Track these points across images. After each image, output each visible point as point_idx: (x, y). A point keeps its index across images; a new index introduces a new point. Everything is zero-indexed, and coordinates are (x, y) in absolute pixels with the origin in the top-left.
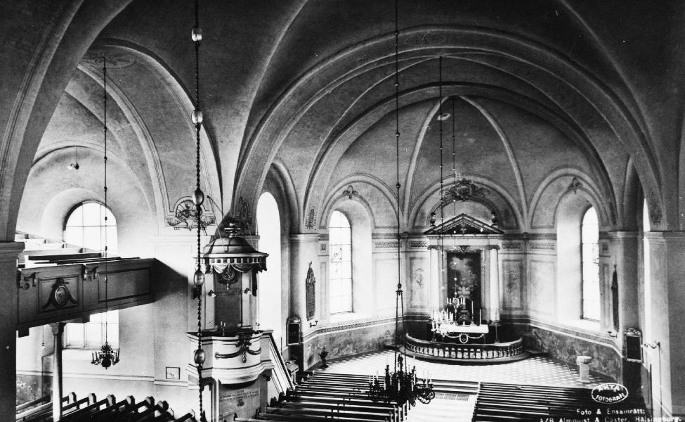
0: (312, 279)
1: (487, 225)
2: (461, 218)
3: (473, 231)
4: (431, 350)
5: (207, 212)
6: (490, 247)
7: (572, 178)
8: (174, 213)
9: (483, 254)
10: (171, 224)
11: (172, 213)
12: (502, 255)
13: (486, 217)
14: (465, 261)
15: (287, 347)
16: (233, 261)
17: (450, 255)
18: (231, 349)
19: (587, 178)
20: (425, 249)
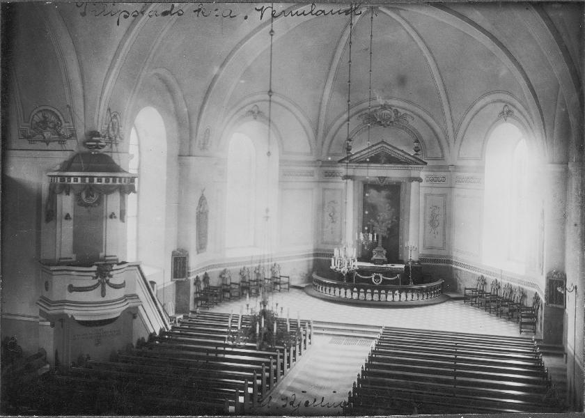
0: (204, 208)
1: (409, 155)
3: (392, 160)
4: (337, 290)
5: (67, 124)
6: (411, 179)
7: (504, 104)
9: (403, 187)
13: (408, 145)
14: (384, 193)
16: (85, 180)
17: (367, 186)
19: (519, 106)
20: (340, 179)
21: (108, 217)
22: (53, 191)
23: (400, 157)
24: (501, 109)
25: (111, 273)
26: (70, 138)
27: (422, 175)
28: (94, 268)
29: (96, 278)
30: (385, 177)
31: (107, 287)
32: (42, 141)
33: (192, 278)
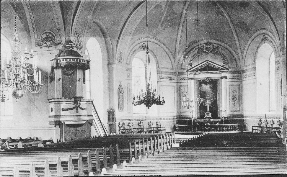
2: (206, 62)
5: (57, 38)
6: (222, 78)
8: (40, 39)
10: (39, 46)
11: (39, 40)
12: (229, 83)
15: (108, 125)
17: (201, 82)
18: (70, 105)
21: (78, 80)
22: (53, 69)
23: (216, 67)
24: (262, 38)
25: (81, 103)
26: (58, 44)
27: (228, 75)
28: (73, 99)
29: (74, 104)
30: (209, 78)
31: (79, 108)
32: (46, 47)
33: (117, 123)
